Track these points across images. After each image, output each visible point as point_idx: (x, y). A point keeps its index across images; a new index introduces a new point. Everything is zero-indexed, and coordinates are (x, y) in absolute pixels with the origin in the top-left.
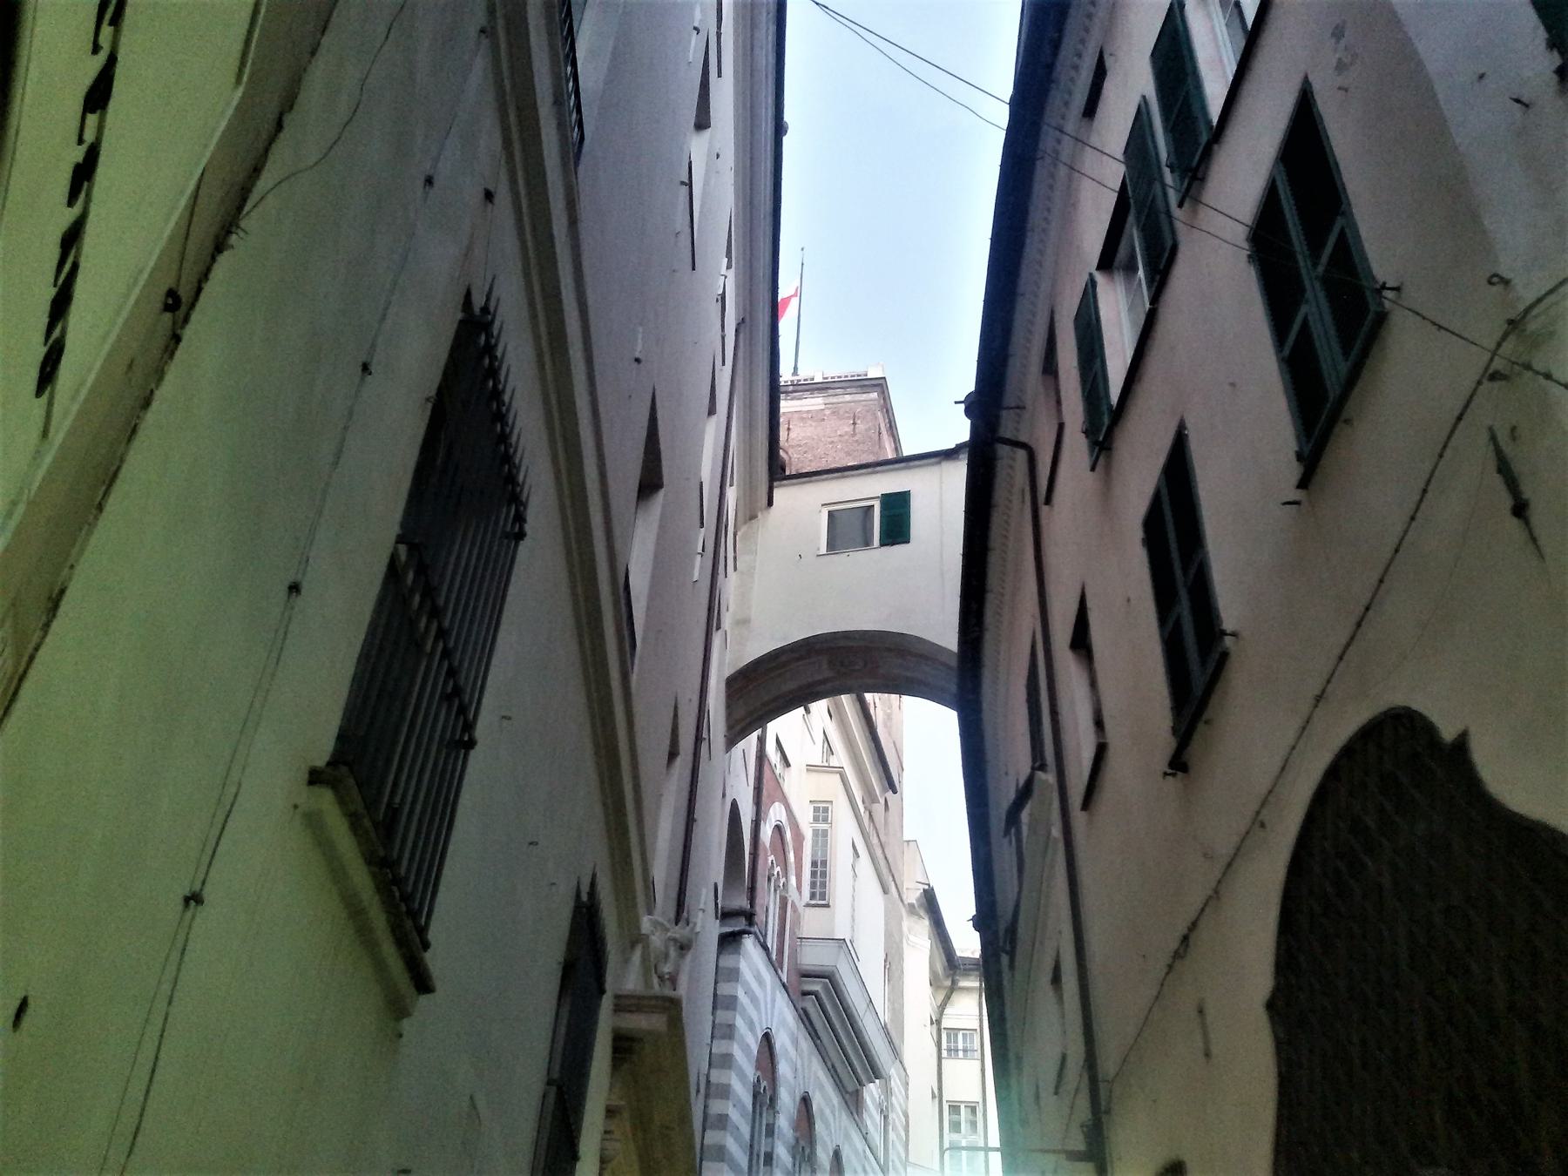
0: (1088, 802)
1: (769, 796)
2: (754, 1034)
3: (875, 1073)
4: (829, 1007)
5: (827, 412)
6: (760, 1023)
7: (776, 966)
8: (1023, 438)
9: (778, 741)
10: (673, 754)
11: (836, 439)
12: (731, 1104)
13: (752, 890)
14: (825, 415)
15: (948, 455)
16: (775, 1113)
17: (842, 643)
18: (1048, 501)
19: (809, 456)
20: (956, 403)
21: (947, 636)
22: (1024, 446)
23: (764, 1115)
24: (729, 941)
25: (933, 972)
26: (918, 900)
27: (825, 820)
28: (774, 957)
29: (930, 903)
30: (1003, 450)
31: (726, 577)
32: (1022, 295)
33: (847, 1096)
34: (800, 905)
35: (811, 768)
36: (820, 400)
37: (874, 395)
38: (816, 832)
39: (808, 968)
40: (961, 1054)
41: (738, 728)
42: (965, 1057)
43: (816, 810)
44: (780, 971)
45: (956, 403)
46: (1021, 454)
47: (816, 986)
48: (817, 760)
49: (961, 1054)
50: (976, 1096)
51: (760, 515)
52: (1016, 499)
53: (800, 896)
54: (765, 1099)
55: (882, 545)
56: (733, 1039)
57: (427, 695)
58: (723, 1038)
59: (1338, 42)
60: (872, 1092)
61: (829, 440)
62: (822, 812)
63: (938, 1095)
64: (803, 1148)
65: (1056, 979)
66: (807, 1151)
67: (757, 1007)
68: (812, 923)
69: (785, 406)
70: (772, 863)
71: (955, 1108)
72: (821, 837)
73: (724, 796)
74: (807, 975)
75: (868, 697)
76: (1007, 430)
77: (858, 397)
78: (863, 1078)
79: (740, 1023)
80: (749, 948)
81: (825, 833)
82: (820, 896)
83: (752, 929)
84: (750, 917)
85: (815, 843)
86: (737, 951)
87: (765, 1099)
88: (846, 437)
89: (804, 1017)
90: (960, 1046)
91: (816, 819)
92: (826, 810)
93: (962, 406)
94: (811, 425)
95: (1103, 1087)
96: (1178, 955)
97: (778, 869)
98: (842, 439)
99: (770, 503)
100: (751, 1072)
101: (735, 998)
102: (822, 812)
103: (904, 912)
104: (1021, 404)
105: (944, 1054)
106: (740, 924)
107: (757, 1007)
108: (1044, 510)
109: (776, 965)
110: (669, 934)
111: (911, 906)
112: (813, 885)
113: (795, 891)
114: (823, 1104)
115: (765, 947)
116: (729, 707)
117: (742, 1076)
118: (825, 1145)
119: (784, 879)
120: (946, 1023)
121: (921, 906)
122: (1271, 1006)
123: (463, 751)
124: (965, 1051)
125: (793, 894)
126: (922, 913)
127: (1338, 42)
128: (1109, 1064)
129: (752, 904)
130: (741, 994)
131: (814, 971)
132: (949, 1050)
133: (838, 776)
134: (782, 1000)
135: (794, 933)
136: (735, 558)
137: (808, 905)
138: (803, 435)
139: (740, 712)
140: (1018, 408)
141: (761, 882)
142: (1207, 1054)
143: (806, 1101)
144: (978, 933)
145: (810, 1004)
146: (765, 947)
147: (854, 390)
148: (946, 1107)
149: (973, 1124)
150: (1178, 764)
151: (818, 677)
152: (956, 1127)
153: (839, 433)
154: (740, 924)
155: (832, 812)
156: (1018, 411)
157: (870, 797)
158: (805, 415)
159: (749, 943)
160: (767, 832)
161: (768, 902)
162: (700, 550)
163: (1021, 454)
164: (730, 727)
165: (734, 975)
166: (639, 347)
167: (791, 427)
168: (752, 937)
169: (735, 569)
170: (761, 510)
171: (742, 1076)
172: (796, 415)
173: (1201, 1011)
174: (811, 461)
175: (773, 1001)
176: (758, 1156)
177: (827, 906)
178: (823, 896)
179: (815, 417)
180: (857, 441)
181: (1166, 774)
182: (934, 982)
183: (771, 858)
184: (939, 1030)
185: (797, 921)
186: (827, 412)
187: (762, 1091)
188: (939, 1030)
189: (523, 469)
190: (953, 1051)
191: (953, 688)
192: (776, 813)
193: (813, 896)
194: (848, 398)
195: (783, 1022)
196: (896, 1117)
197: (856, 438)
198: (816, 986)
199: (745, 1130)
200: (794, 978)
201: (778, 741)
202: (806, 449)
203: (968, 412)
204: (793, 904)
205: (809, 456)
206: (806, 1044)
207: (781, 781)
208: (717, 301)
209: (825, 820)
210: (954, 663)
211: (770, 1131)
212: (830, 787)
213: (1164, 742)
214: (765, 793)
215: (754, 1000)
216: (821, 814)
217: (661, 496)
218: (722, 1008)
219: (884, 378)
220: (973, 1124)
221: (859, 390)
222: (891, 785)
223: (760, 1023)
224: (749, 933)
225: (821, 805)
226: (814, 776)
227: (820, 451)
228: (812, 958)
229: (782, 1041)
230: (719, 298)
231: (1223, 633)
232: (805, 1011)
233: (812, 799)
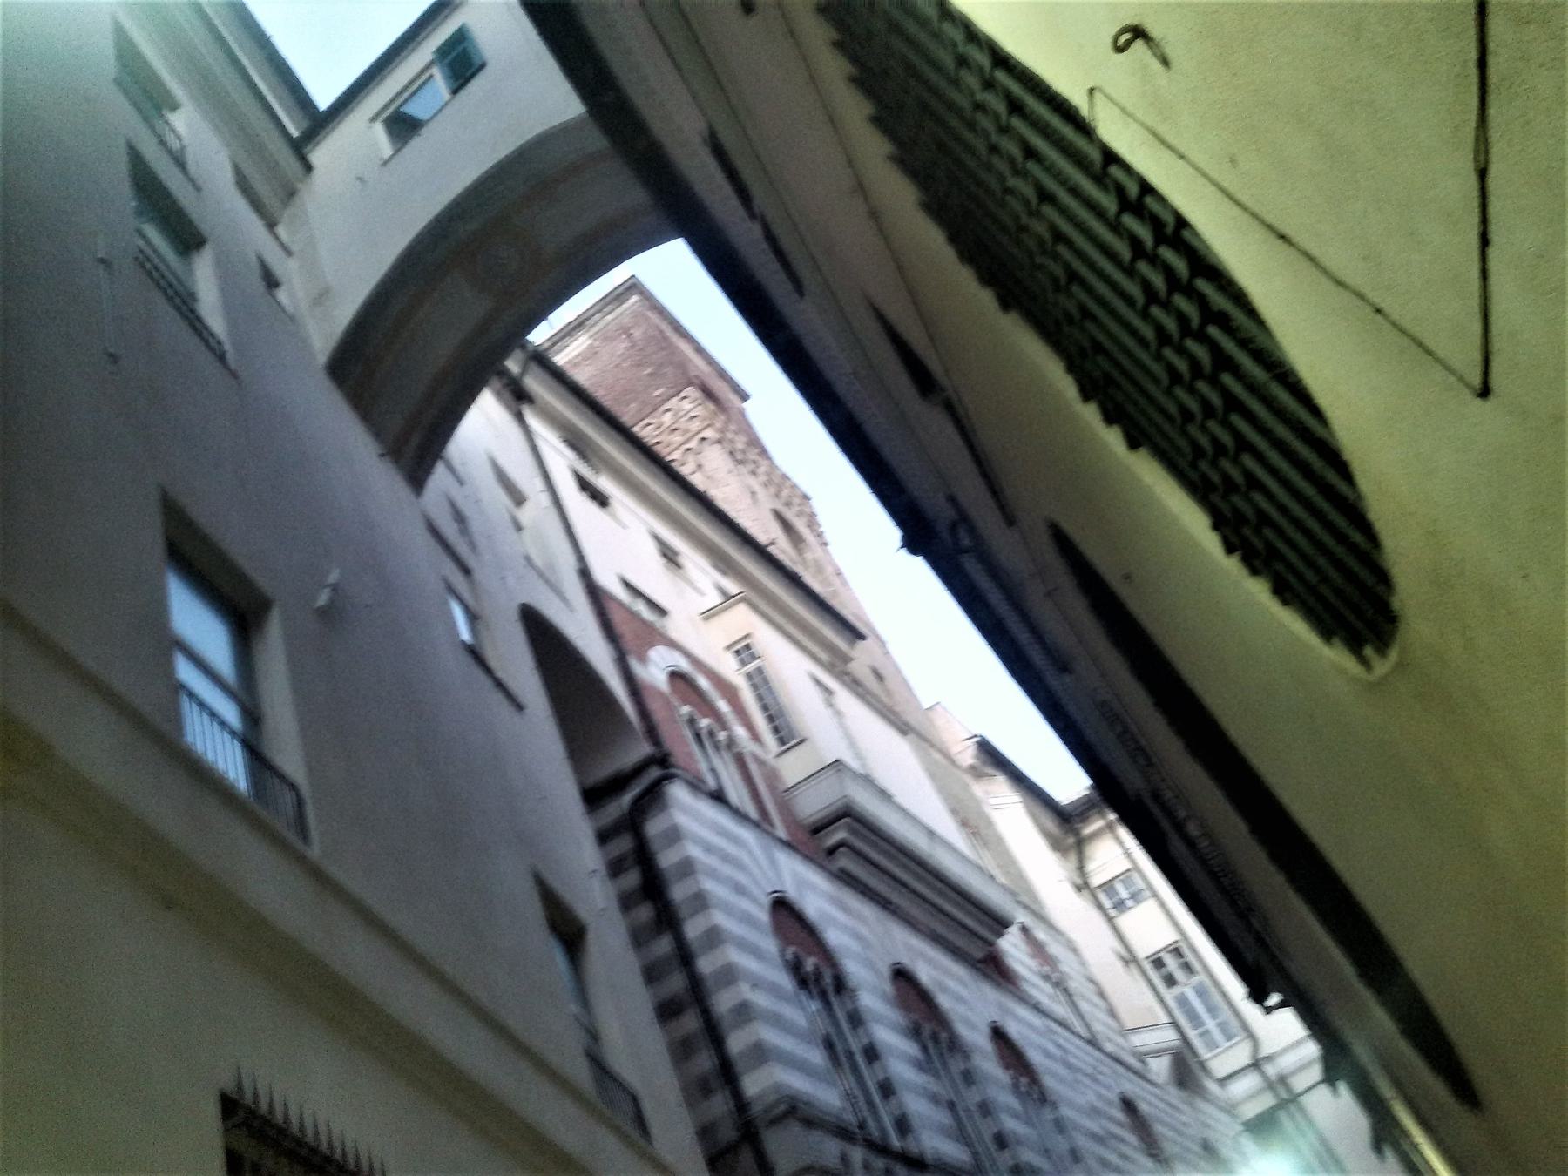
3: (1001, 924)
4: (874, 855)
13: (652, 732)
16: (852, 993)
25: (1047, 835)
26: (977, 757)
27: (754, 657)
29: (991, 758)
31: (198, 189)
33: (979, 965)
36: (582, 339)
37: (634, 299)
38: (749, 676)
39: (812, 819)
40: (1129, 903)
42: (1138, 902)
47: (838, 835)
50: (1169, 936)
51: (299, 186)
55: (455, 92)
56: (983, 1100)
58: (694, 913)
60: (1011, 946)
62: (744, 651)
63: (1129, 959)
68: (793, 768)
71: (1158, 963)
72: (760, 681)
74: (818, 829)
77: (619, 310)
78: (988, 935)
81: (760, 670)
82: (787, 735)
84: (662, 760)
85: (755, 687)
89: (846, 879)
91: (743, 663)
92: (748, 647)
99: (308, 168)
102: (744, 651)
103: (968, 779)
105: (1113, 913)
106: (654, 773)
111: (972, 768)
112: (776, 730)
118: (973, 1027)
120: (1096, 880)
121: (984, 763)
126: (990, 770)
131: (827, 816)
135: (776, 788)
143: (902, 976)
145: (844, 861)
147: (610, 307)
148: (1148, 966)
149: (1187, 967)
152: (1170, 981)
154: (654, 773)
159: (678, 792)
169: (288, 252)
170: (302, 182)
179: (590, 354)
182: (1057, 845)
184: (1139, 966)
185: (772, 777)
188: (1139, 966)
190: (1120, 906)
193: (782, 741)
194: (609, 317)
195: (802, 883)
196: (1077, 984)
198: (838, 835)
209: (754, 657)
212: (742, 620)
219: (633, 276)
220: (1187, 967)
221: (616, 303)
222: (855, 634)
224: (669, 777)
225: (739, 646)
226: (716, 622)
228: (812, 805)
232: (843, 871)
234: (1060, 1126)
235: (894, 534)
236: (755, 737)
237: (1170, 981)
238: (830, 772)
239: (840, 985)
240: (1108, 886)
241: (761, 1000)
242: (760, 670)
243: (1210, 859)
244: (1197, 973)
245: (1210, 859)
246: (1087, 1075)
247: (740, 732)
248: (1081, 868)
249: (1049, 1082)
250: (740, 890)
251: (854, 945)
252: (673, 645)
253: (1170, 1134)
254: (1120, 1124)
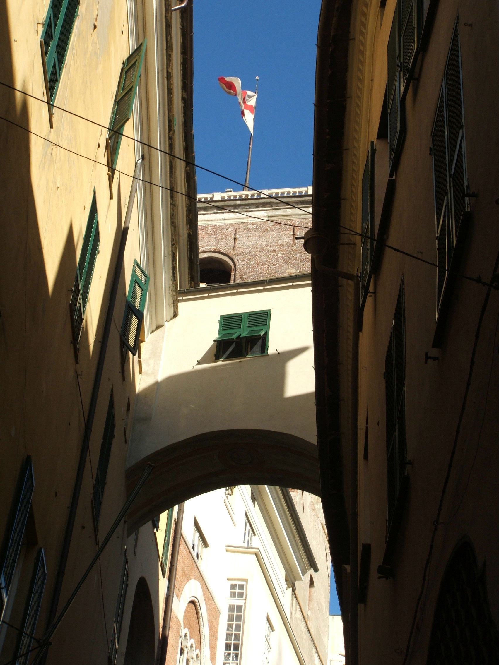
9: (196, 524)
11: (277, 248)
14: (268, 227)
19: (253, 263)
27: (241, 595)
35: (230, 549)
38: (231, 608)
43: (233, 587)
48: (239, 542)
57: (236, 317)
59: (197, 365)
61: (271, 249)
70: (186, 635)
75: (296, 495)
85: (231, 618)
88: (287, 247)
91: (233, 595)
92: (241, 587)
94: (255, 236)
97: (192, 641)
98: (282, 248)
122: (56, 46)
123: (310, 282)
127: (197, 365)
133: (255, 555)
138: (248, 244)
153: (280, 242)
155: (247, 588)
158: (250, 226)
167: (237, 236)
172: (242, 226)
174: (254, 267)
180: (295, 250)
183: (185, 631)
197: (295, 248)
201: (196, 524)
202: (250, 257)
205: (253, 263)
216: (235, 613)
227: (263, 259)
242: (240, 608)
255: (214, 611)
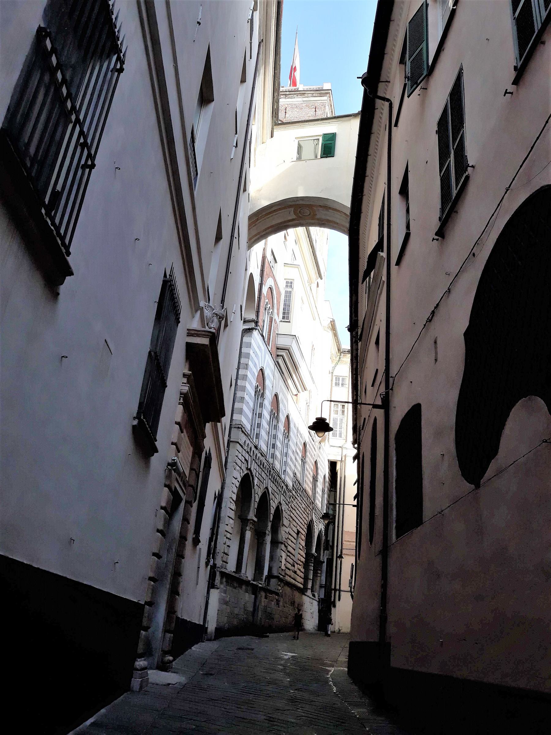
0: (398, 263)
1: (267, 274)
2: (256, 369)
5: (304, 105)
6: (259, 365)
7: (267, 344)
8: (387, 97)
10: (219, 237)
12: (246, 394)
15: (354, 115)
17: (301, 202)
18: (396, 125)
20: (358, 78)
21: (346, 201)
22: (388, 100)
23: (285, 440)
24: (248, 331)
28: (266, 340)
30: (378, 102)
32: (393, 21)
34: (278, 321)
38: (286, 292)
40: (340, 385)
41: (253, 240)
43: (287, 282)
44: (268, 346)
45: (358, 78)
46: (387, 104)
49: (340, 385)
52: (382, 129)
53: (277, 318)
54: (260, 393)
55: (321, 157)
62: (290, 284)
64: (274, 413)
65: (377, 342)
66: (276, 415)
67: (258, 359)
69: (283, 101)
72: (288, 295)
73: (246, 270)
76: (380, 93)
79: (250, 363)
80: (255, 335)
82: (286, 317)
83: (257, 328)
84: (256, 323)
85: (286, 296)
86: (251, 336)
87: (260, 393)
90: (341, 382)
91: (287, 286)
93: (361, 80)
95: (391, 380)
96: (430, 320)
100: (254, 383)
101: (249, 354)
104: (388, 80)
106: (253, 325)
107: (258, 359)
108: (394, 129)
109: (267, 343)
110: (214, 311)
112: (284, 313)
113: (276, 314)
114: (283, 397)
115: (262, 336)
116: (249, 229)
117: (251, 384)
118: (283, 414)
119: (272, 310)
124: (342, 385)
125: (275, 317)
128: (394, 371)
129: (257, 316)
130: (251, 353)
132: (336, 384)
134: (268, 358)
136: (255, 160)
137: (281, 321)
139: (254, 232)
140: (387, 82)
141: (262, 309)
142: (436, 360)
143: (276, 396)
144: (349, 333)
145: (280, 361)
146: (262, 336)
149: (343, 412)
150: (441, 233)
151: (290, 218)
154: (253, 325)
156: (387, 83)
157: (310, 282)
159: (255, 333)
160: (265, 290)
161: (264, 318)
162: (235, 145)
163: (387, 104)
164: (250, 239)
165: (249, 345)
166: (200, 17)
168: (257, 331)
171: (251, 384)
173: (435, 342)
175: (265, 358)
176: (256, 414)
177: (289, 322)
178: (288, 318)
181: (433, 239)
186: (304, 105)
187: (259, 390)
189: (121, 39)
191: (348, 225)
192: (269, 282)
193: (283, 318)
195: (268, 365)
199: (251, 404)
200: (274, 349)
203: (363, 83)
204: (275, 319)
206: (277, 374)
207: (273, 269)
208: (248, 22)
209: (291, 286)
210: (348, 212)
211: (261, 405)
213: (435, 224)
214: (265, 273)
215: (256, 355)
217: (212, 105)
218: (243, 358)
220: (343, 412)
223: (259, 365)
228: (282, 342)
229: (267, 372)
230: (249, 21)
231: (468, 166)
232: (278, 362)
233: (285, 278)
234: (287, 446)
235: (348, 323)
236: (278, 314)
237: (337, 412)
238: (292, 337)
239: (263, 395)
240: (337, 378)
241: (247, 397)
243: (302, 562)
244: (329, 461)
245: (302, 562)
246: (291, 710)
247: (275, 311)
248: (334, 368)
249: (291, 434)
250: (255, 365)
251: (270, 386)
252: (275, 280)
253: (310, 456)
254: (300, 449)
255: (279, 293)
